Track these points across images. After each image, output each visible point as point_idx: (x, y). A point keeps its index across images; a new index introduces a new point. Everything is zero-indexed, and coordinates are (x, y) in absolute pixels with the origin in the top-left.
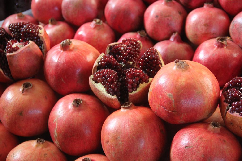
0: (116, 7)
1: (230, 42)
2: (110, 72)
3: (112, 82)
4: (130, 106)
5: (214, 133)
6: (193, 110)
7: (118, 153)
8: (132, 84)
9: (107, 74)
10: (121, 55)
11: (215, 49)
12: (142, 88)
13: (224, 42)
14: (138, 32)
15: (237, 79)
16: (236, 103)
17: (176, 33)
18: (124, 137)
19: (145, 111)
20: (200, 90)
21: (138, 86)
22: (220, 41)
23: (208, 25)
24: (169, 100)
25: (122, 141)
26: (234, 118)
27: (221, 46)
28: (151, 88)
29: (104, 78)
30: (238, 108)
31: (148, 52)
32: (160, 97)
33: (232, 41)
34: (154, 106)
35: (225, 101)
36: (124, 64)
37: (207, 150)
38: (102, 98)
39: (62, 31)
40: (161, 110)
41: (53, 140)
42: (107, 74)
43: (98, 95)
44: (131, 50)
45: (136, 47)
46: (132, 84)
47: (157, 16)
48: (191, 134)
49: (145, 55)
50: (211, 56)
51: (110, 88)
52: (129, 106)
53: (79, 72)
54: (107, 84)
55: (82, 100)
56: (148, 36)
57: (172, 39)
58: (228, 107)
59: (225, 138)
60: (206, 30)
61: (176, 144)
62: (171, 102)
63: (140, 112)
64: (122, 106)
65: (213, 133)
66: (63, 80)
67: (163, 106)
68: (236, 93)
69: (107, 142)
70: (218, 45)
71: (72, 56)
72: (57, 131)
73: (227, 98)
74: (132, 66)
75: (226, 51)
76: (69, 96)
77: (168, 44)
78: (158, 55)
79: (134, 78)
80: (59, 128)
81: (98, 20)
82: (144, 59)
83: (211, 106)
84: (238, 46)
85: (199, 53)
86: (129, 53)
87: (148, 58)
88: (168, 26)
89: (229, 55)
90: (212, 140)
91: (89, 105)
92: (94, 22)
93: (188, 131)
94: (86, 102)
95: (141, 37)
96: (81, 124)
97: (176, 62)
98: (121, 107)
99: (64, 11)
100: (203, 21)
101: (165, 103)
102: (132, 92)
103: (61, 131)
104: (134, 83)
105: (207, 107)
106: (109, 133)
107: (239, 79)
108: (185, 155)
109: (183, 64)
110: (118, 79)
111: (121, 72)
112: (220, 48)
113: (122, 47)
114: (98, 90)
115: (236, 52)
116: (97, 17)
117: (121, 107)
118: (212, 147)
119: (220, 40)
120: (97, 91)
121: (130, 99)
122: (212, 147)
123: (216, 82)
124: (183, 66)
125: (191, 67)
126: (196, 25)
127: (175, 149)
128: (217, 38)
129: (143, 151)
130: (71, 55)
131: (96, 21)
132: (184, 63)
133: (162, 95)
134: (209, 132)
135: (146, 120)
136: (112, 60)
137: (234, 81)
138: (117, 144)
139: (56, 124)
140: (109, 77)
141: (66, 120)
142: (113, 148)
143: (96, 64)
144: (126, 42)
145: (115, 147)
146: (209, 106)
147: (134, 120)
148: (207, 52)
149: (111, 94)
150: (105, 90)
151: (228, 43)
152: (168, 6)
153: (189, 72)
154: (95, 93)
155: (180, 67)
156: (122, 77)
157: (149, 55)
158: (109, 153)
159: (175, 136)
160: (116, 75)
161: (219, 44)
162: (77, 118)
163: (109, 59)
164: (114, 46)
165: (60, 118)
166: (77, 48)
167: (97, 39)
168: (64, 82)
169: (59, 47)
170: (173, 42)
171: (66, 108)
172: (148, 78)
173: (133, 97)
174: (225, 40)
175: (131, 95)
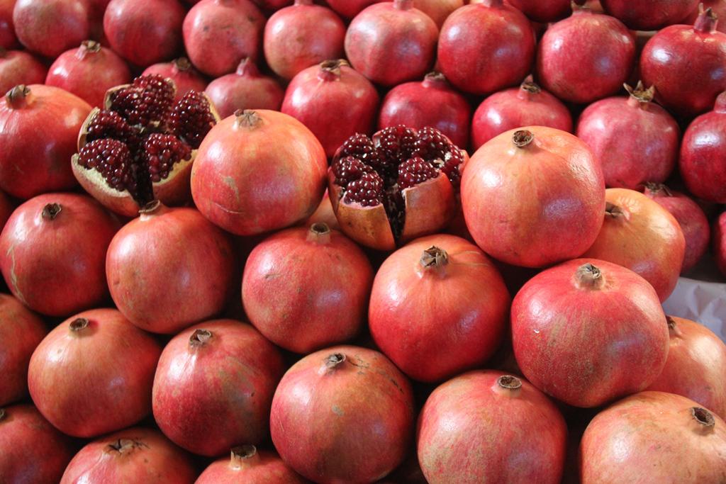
0: (124, 14)
1: (347, 70)
2: (111, 145)
3: (116, 164)
4: (157, 208)
5: (319, 244)
6: (277, 204)
7: (140, 301)
8: (158, 165)
9: (105, 149)
10: (135, 109)
11: (320, 84)
12: (178, 172)
13: (335, 71)
14: (173, 61)
15: (357, 139)
16: (354, 184)
17: (247, 59)
18: (149, 270)
19: (187, 215)
20: (286, 165)
21: (169, 168)
22: (328, 69)
23: (305, 39)
24: (229, 189)
25: (145, 279)
26: (352, 212)
27: (330, 78)
28: (194, 171)
29: (100, 157)
30: (358, 193)
31: (185, 99)
32: (212, 185)
33: (351, 66)
34: (203, 204)
35: (335, 183)
36: (143, 126)
37: (307, 278)
38: (101, 198)
39: (20, 70)
40: (216, 211)
41: (11, 289)
42: (105, 149)
43: (92, 192)
44: (153, 98)
45: (164, 92)
46: (158, 165)
47: (206, 28)
48: (276, 252)
49: (181, 106)
50: (313, 99)
51: (114, 176)
52: (155, 208)
53: (51, 150)
54: (107, 169)
55: (60, 206)
56: (193, 67)
57: (240, 72)
58: (342, 193)
59: (339, 252)
60: (303, 48)
61: (250, 274)
62: (232, 193)
63: (178, 218)
64: (141, 209)
65: (317, 246)
66: (18, 169)
67: (220, 204)
68: (354, 164)
69: (117, 283)
70: (324, 76)
71: (32, 119)
72: (15, 271)
73: (339, 177)
74: (159, 130)
75: (339, 88)
76: (35, 200)
77: (233, 81)
78: (207, 103)
79: (161, 154)
80: (19, 264)
81: (91, 44)
82: (180, 113)
83: (310, 194)
84: (361, 76)
85: (291, 94)
86: (150, 103)
87: (186, 110)
88: (231, 45)
89: (346, 95)
90: (315, 259)
91: (76, 213)
92: (83, 48)
93: (270, 247)
94: (69, 209)
95: (180, 71)
96: (63, 253)
97: (237, 115)
98: (140, 211)
99: (19, 28)
100: (295, 32)
101: (221, 197)
102: (160, 180)
103: (23, 270)
104: (161, 162)
105: (303, 197)
106: (118, 266)
107: (359, 138)
108: (266, 292)
109: (250, 117)
110: (132, 156)
111: (135, 145)
112: (328, 82)
113: (134, 92)
114: (91, 183)
115: (360, 88)
116: (90, 37)
117: (140, 211)
118: (316, 272)
119: (328, 66)
120: (90, 185)
121: (156, 196)
122: (316, 272)
123: (317, 148)
124: (252, 121)
125: (266, 123)
126: (282, 40)
127: (249, 282)
128: (322, 64)
129: (188, 293)
130: (31, 115)
131: (87, 45)
132: (254, 115)
133: (214, 182)
134: (309, 243)
135: (190, 234)
136: (115, 121)
137: (350, 143)
138: (135, 285)
139: (11, 258)
140: (110, 154)
141: (31, 248)
142: (129, 294)
143: (83, 131)
144: (142, 82)
145: (132, 292)
146: (307, 194)
147: (166, 235)
148: (306, 91)
149: (117, 189)
150: (105, 182)
151: (342, 73)
152: (226, 6)
153: (263, 133)
154: (86, 189)
155: (246, 123)
156: (140, 154)
157: (188, 105)
158: (123, 303)
159: (249, 259)
160: (123, 150)
161: (326, 74)
162: (53, 243)
163: (108, 119)
164: (118, 91)
165: (20, 247)
166: (43, 103)
167: (92, 81)
168: (22, 173)
169: (5, 102)
170: (242, 76)
171: (30, 224)
172: (189, 150)
173: (163, 190)
174: (337, 67)
175: (159, 187)
